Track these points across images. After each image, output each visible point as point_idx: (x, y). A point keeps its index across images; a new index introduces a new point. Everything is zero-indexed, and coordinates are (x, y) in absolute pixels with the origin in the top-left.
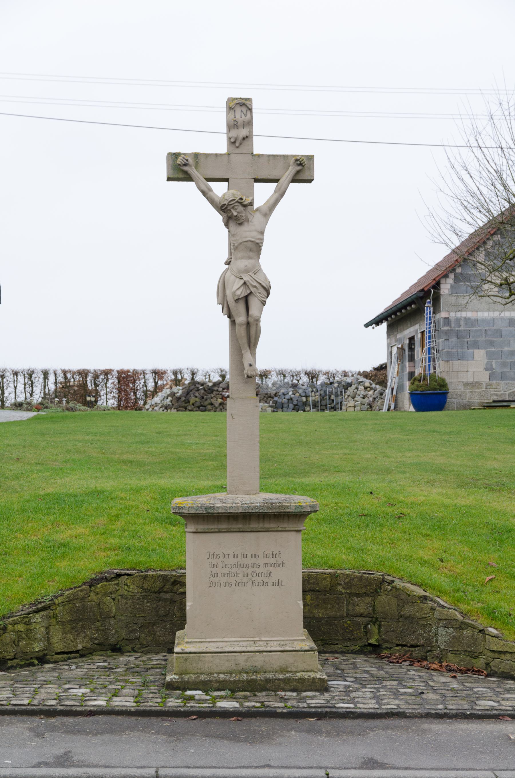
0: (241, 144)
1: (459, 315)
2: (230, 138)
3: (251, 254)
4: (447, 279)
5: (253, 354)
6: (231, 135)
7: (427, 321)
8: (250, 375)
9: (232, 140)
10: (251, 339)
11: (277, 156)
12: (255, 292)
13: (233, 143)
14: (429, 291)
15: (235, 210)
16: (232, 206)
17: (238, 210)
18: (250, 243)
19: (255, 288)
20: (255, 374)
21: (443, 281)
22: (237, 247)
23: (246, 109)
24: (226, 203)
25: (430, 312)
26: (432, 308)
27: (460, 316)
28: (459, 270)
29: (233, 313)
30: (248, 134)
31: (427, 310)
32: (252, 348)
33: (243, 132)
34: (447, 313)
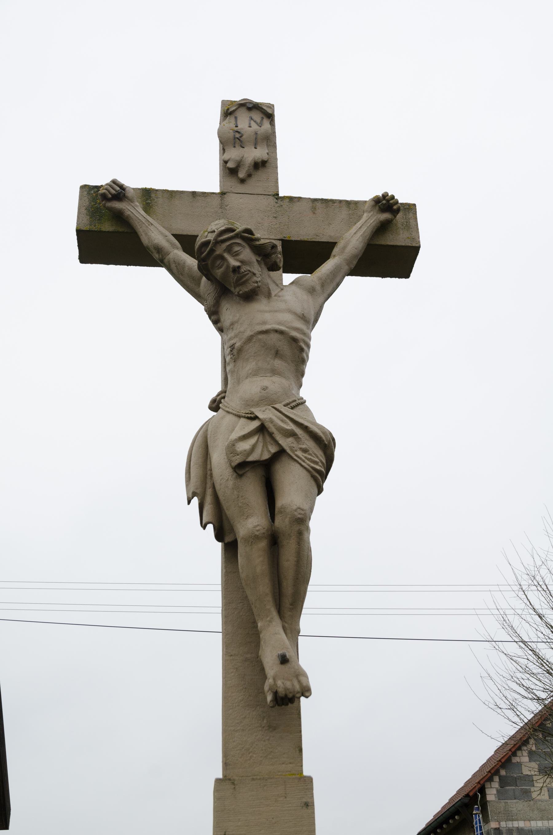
0: (249, 176)
1: (510, 824)
2: (226, 162)
3: (278, 363)
4: (492, 783)
5: (292, 631)
6: (226, 157)
7: (477, 831)
8: (281, 692)
9: (230, 165)
10: (284, 584)
11: (333, 201)
12: (291, 448)
13: (230, 171)
14: (475, 795)
15: (235, 255)
16: (228, 243)
17: (241, 257)
18: (274, 337)
19: (291, 439)
20: (297, 687)
21: (487, 785)
22: (240, 351)
23: (261, 115)
24: (211, 237)
25: (479, 820)
26: (481, 816)
27: (511, 826)
28: (503, 772)
29: (231, 511)
30: (265, 157)
31: (476, 818)
32: (288, 614)
33: (252, 154)
34: (497, 823)
